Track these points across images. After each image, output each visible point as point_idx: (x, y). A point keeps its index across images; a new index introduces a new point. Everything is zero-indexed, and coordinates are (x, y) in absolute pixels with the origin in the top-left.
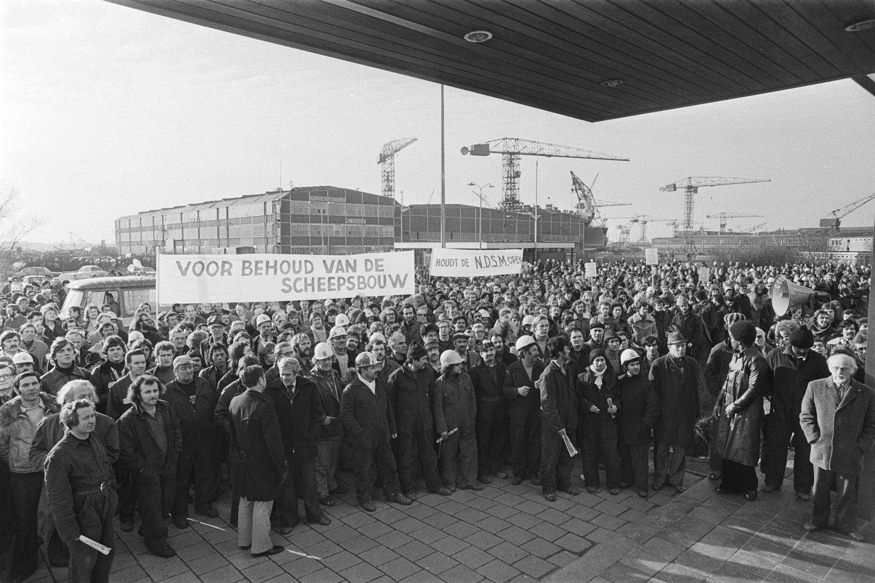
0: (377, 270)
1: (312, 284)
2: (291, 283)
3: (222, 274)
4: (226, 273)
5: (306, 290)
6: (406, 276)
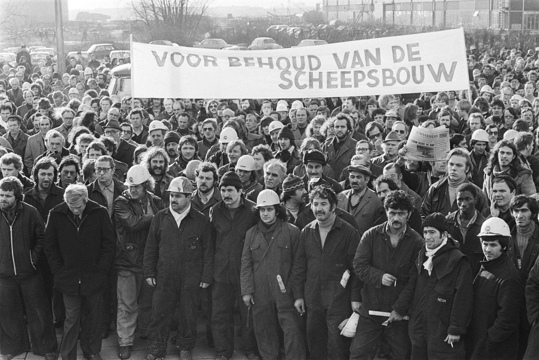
0: (411, 59)
1: (320, 80)
2: (292, 78)
3: (206, 65)
4: (210, 63)
5: (311, 86)
6: (454, 64)
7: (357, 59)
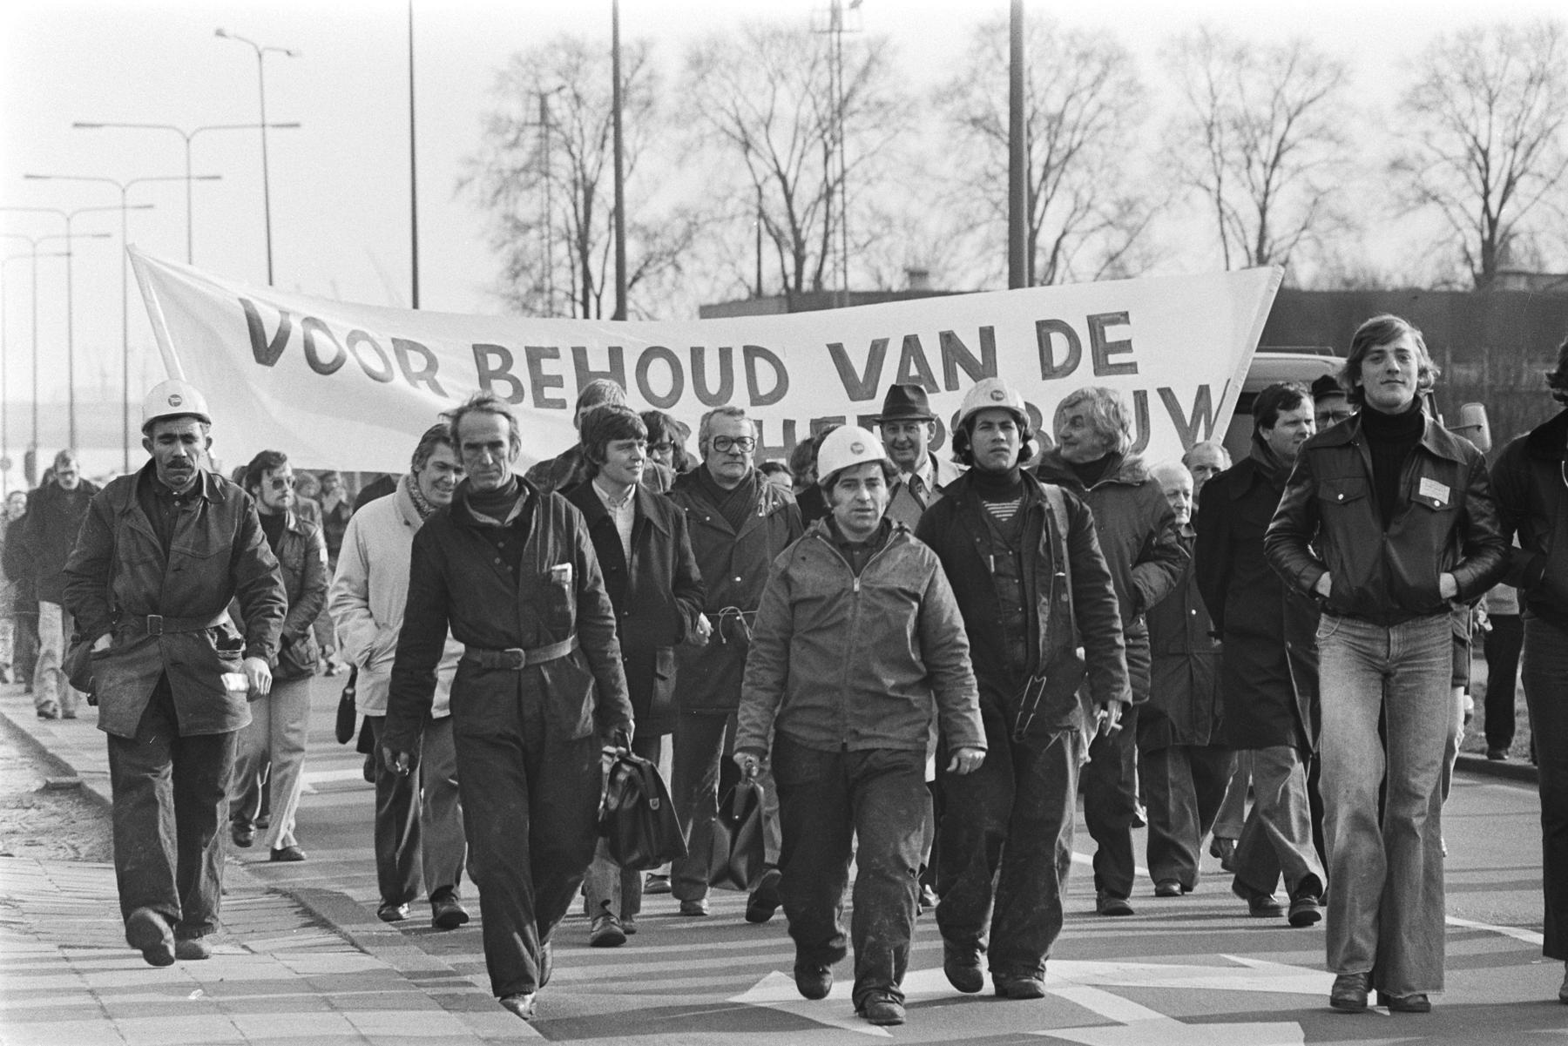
0: (1101, 368)
7: (913, 365)
